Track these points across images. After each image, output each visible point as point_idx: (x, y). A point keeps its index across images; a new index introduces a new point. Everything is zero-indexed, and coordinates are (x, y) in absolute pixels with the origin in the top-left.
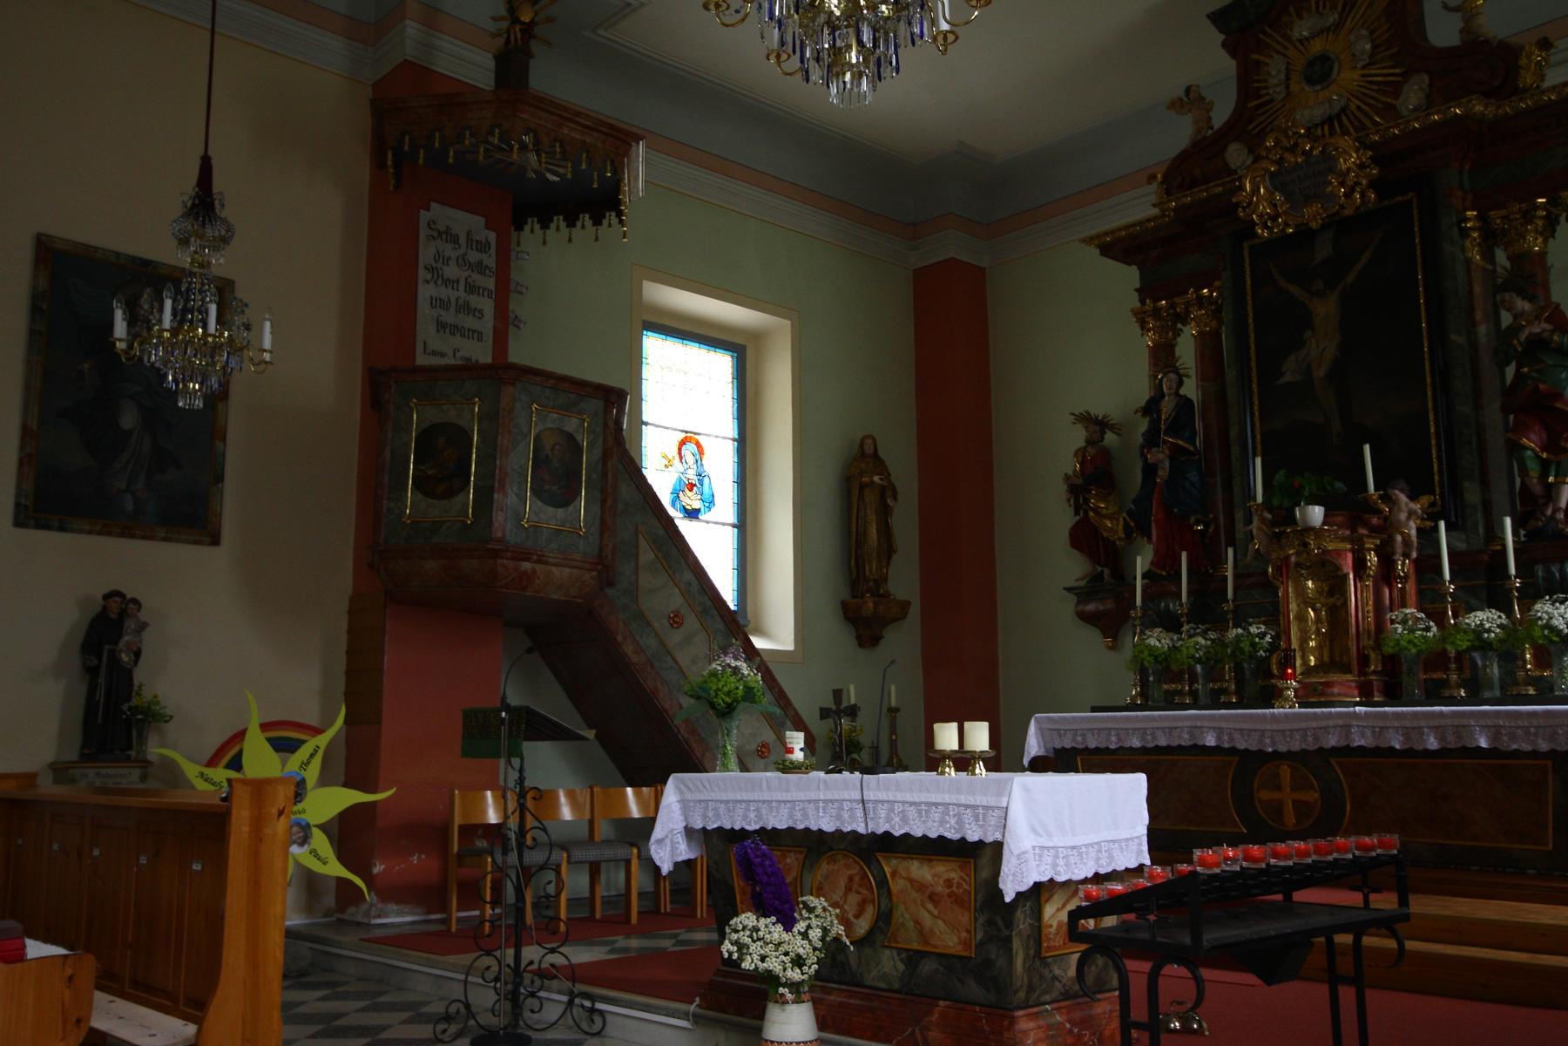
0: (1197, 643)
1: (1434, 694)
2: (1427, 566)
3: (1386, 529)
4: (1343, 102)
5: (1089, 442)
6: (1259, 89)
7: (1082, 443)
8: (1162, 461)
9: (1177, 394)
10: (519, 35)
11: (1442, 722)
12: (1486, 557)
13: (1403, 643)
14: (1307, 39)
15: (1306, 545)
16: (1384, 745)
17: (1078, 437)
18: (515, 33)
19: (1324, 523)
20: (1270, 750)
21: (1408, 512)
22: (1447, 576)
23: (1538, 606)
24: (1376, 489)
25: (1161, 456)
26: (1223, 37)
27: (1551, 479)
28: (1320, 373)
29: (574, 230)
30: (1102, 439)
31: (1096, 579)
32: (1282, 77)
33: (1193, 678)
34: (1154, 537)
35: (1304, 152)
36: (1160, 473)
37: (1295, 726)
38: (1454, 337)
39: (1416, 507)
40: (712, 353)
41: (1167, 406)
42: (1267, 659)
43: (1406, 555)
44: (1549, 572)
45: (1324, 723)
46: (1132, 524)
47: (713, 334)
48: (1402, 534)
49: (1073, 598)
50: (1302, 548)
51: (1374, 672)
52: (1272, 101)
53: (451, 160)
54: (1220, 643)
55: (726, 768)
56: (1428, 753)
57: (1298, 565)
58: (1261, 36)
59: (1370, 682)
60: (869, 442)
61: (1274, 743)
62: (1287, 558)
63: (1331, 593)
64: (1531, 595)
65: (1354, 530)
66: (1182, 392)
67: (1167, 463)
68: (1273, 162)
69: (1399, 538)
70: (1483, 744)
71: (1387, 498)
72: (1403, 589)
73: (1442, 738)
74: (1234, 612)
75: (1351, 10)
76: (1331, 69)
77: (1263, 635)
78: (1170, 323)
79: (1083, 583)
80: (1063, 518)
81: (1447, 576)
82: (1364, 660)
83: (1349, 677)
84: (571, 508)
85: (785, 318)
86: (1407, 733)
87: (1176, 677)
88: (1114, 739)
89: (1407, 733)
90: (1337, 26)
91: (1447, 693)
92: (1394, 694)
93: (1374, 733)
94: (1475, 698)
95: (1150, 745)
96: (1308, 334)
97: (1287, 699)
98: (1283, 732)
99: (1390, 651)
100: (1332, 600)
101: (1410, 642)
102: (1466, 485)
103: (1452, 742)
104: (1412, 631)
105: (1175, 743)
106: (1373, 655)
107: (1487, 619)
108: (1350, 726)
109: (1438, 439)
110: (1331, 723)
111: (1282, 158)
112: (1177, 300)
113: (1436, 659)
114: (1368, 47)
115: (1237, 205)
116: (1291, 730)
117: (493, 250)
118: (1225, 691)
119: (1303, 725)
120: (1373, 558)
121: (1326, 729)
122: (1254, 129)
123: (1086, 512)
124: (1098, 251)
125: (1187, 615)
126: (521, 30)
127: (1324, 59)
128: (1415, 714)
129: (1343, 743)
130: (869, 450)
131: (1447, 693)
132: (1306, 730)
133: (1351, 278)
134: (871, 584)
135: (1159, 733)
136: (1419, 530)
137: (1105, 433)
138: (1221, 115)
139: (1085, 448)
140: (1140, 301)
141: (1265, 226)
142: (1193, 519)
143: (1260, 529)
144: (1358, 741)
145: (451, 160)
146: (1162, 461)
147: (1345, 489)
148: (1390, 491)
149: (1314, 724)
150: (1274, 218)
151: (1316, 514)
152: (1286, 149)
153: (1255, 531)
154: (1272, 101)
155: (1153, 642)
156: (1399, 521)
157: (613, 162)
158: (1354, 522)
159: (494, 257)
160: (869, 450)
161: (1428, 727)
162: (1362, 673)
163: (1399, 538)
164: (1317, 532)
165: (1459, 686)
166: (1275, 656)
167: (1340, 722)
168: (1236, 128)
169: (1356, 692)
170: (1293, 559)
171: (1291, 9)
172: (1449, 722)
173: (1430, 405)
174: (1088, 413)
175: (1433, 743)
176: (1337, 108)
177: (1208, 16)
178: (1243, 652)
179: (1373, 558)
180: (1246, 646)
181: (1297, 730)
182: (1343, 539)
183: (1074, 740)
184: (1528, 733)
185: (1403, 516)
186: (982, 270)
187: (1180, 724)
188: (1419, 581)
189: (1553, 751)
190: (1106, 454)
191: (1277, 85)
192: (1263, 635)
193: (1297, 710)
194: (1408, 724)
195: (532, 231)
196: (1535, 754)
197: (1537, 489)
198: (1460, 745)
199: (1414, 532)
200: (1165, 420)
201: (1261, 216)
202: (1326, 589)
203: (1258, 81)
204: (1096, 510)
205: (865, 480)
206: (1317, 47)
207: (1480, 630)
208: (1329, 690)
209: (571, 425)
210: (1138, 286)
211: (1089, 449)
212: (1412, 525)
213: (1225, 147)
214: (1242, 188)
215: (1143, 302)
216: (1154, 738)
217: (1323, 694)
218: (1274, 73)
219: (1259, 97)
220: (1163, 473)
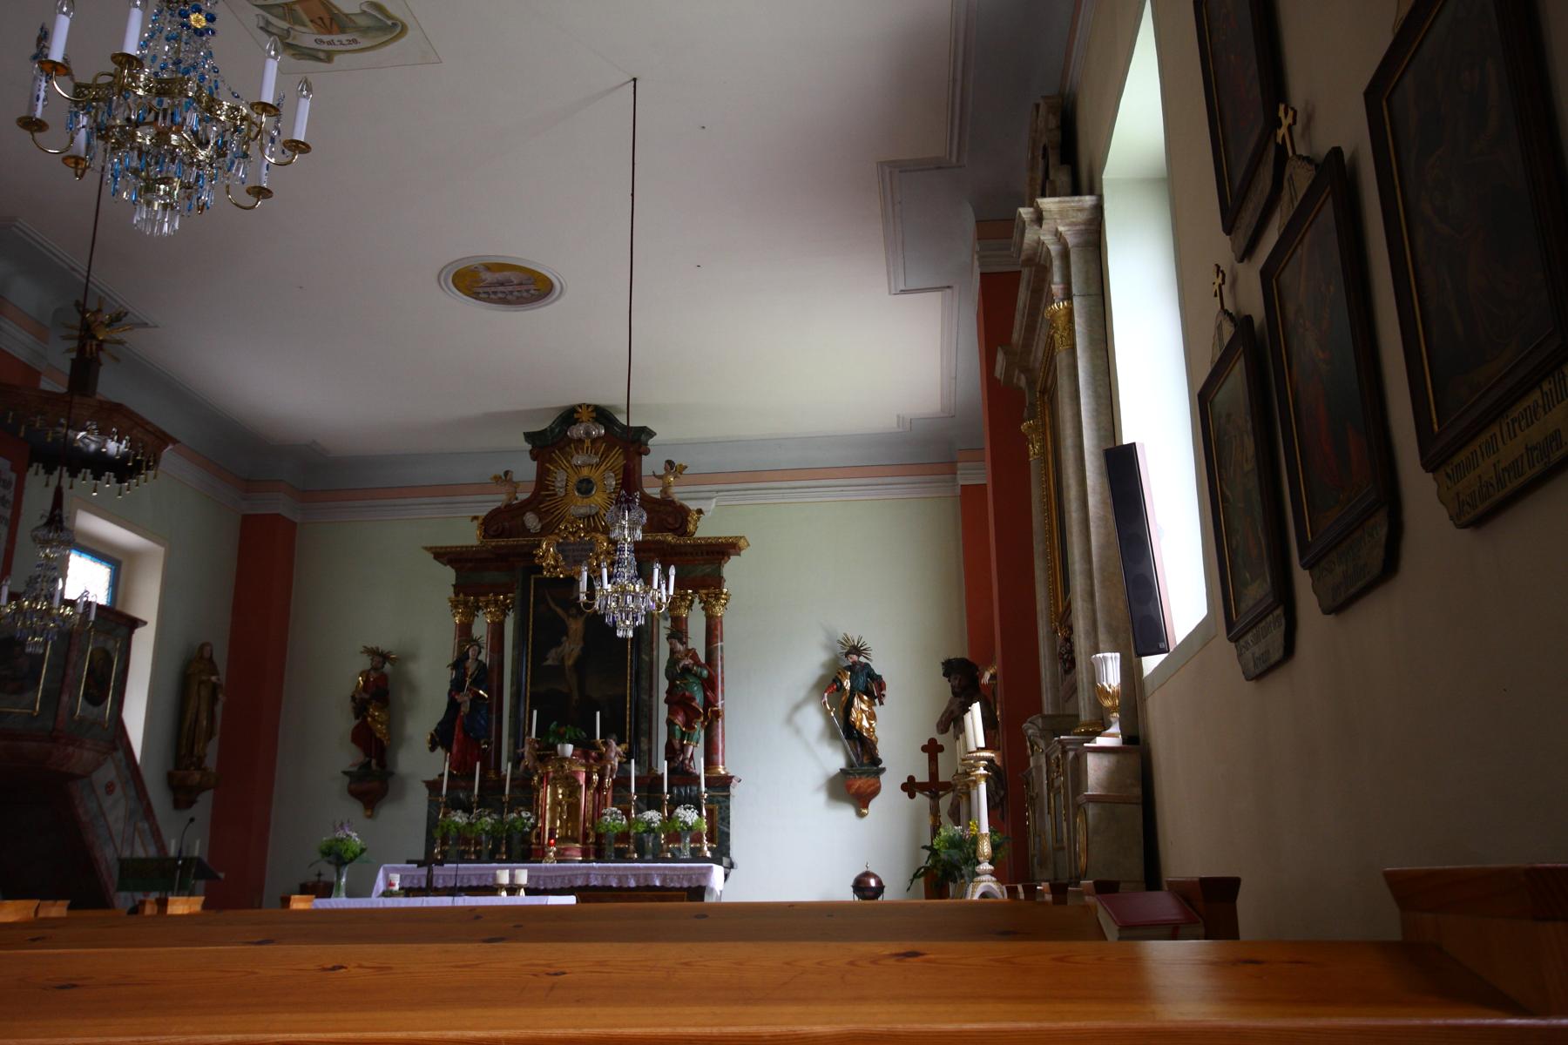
0: (487, 821)
1: (621, 856)
2: (621, 783)
3: (602, 758)
4: (598, 510)
5: (374, 668)
6: (548, 485)
7: (368, 667)
8: (465, 702)
9: (477, 659)
10: (94, 347)
11: (638, 872)
12: (649, 781)
13: (611, 827)
14: (580, 466)
15: (563, 767)
16: (607, 884)
17: (365, 663)
18: (91, 345)
19: (572, 755)
20: (542, 888)
21: (616, 751)
22: (633, 791)
23: (678, 810)
24: (601, 738)
25: (466, 698)
26: (917, 781)
27: (685, 742)
28: (569, 662)
29: (75, 480)
30: (383, 667)
31: (366, 766)
32: (564, 483)
33: (478, 843)
34: (455, 748)
35: (580, 537)
36: (463, 709)
37: (558, 874)
38: (644, 656)
39: (619, 749)
40: (98, 565)
41: (471, 666)
42: (530, 833)
43: (611, 776)
44: (679, 791)
45: (575, 872)
46: (437, 739)
47: (102, 550)
48: (611, 764)
49: (347, 779)
50: (560, 769)
51: (591, 843)
52: (555, 495)
53: (10, 421)
54: (501, 821)
55: (338, 896)
56: (630, 889)
57: (554, 778)
58: (554, 455)
59: (589, 849)
60: (208, 648)
61: (544, 884)
62: (548, 773)
63: (570, 796)
64: (675, 803)
65: (587, 760)
66: (480, 658)
67: (468, 703)
68: (563, 538)
69: (609, 767)
70: (658, 883)
71: (606, 744)
72: (606, 795)
73: (637, 881)
74: (508, 803)
75: (606, 457)
76: (592, 489)
77: (528, 819)
78: (470, 612)
79: (355, 769)
80: (344, 722)
81: (633, 791)
82: (586, 836)
83: (578, 845)
84: (102, 707)
85: (158, 543)
86: (620, 878)
87: (467, 842)
88: (441, 881)
89: (620, 878)
90: (598, 465)
91: (628, 856)
92: (600, 857)
93: (602, 878)
94: (641, 859)
95: (466, 885)
96: (564, 638)
97: (549, 858)
98: (551, 877)
99: (602, 831)
100: (570, 800)
101: (614, 826)
102: (643, 739)
103: (642, 884)
104: (614, 820)
105: (483, 884)
106: (592, 833)
107: (653, 815)
108: (589, 874)
109: (631, 711)
110: (579, 872)
111: (567, 537)
112: (482, 599)
113: (624, 836)
114: (614, 483)
115: (536, 555)
116: (556, 876)
117: (12, 489)
118: (468, 852)
119: (564, 873)
120: (595, 777)
121: (576, 876)
123: (365, 718)
124: (432, 556)
125: (477, 803)
126: (97, 345)
127: (588, 481)
128: (625, 868)
129: (585, 884)
130: (206, 655)
131: (628, 856)
132: (564, 876)
134: (195, 759)
135: (472, 878)
136: (619, 763)
137: (385, 663)
138: (523, 496)
139: (369, 671)
140: (455, 593)
141: (549, 571)
142: (482, 742)
143: (529, 753)
144: (594, 883)
145: (10, 421)
146: (465, 702)
147: (992, 868)
148: (608, 740)
149: (569, 873)
150: (555, 567)
151: (569, 748)
152: (570, 532)
153: (526, 754)
154: (555, 495)
155: (457, 819)
156: (610, 757)
157: (155, 456)
158: (586, 756)
159: (12, 494)
160: (206, 655)
161: (632, 875)
162: (584, 843)
163: (609, 767)
164: (570, 760)
165: (634, 852)
166: (535, 832)
167: (585, 871)
168: (531, 504)
169: (580, 854)
170: (551, 775)
171: (572, 446)
172: (642, 872)
173: (628, 692)
174: (378, 649)
175: (633, 884)
176: (594, 512)
177: (524, 433)
178: (516, 829)
179: (595, 777)
180: (518, 824)
181: (559, 876)
182: (582, 765)
183: (411, 882)
184: (679, 878)
185: (613, 755)
186: (295, 524)
187: (487, 872)
188: (614, 791)
189: (689, 887)
190: (383, 678)
191: (561, 488)
192: (528, 819)
193: (555, 864)
194: (620, 873)
195: (36, 474)
196: (681, 889)
197: (677, 746)
198: (646, 884)
199: (617, 764)
200: (471, 675)
201: (548, 564)
202: (568, 793)
203: (549, 481)
204: (373, 717)
205: (204, 678)
206: (585, 472)
207: (650, 822)
208: (568, 853)
209: (110, 645)
210: (454, 583)
211: (372, 672)
212: (617, 760)
213: (524, 513)
214: (539, 546)
215: (457, 594)
216: (469, 880)
217: (563, 855)
218: (559, 479)
219: (548, 490)
220: (465, 709)
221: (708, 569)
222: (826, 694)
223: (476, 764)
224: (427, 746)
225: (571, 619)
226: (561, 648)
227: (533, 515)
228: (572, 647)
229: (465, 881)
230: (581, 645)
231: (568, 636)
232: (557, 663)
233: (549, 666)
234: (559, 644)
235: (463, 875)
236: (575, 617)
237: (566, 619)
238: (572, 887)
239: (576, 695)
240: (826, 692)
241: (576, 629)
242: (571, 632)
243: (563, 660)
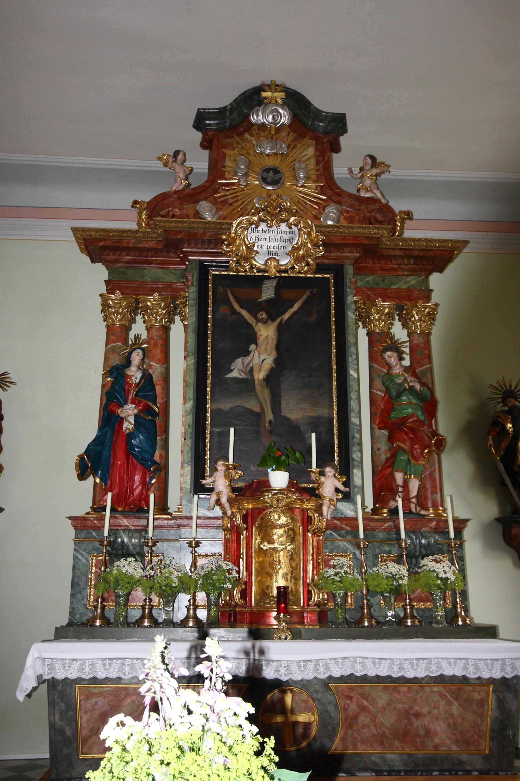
23: (425, 561)
28: (260, 376)
36: (125, 425)
96: (253, 347)
122: (220, 197)
133: (286, 316)
221: (413, 281)
222: (490, 437)
223: (310, 437)
224: (74, 474)
225: (259, 324)
226: (249, 358)
227: (208, 204)
228: (262, 358)
229: (87, 669)
230: (274, 355)
231: (257, 344)
232: (243, 376)
233: (236, 379)
234: (247, 353)
235: (280, 661)
236: (264, 322)
237: (254, 325)
238: (442, 676)
239: (269, 416)
240: (488, 434)
241: (267, 337)
242: (260, 340)
243: (251, 371)
